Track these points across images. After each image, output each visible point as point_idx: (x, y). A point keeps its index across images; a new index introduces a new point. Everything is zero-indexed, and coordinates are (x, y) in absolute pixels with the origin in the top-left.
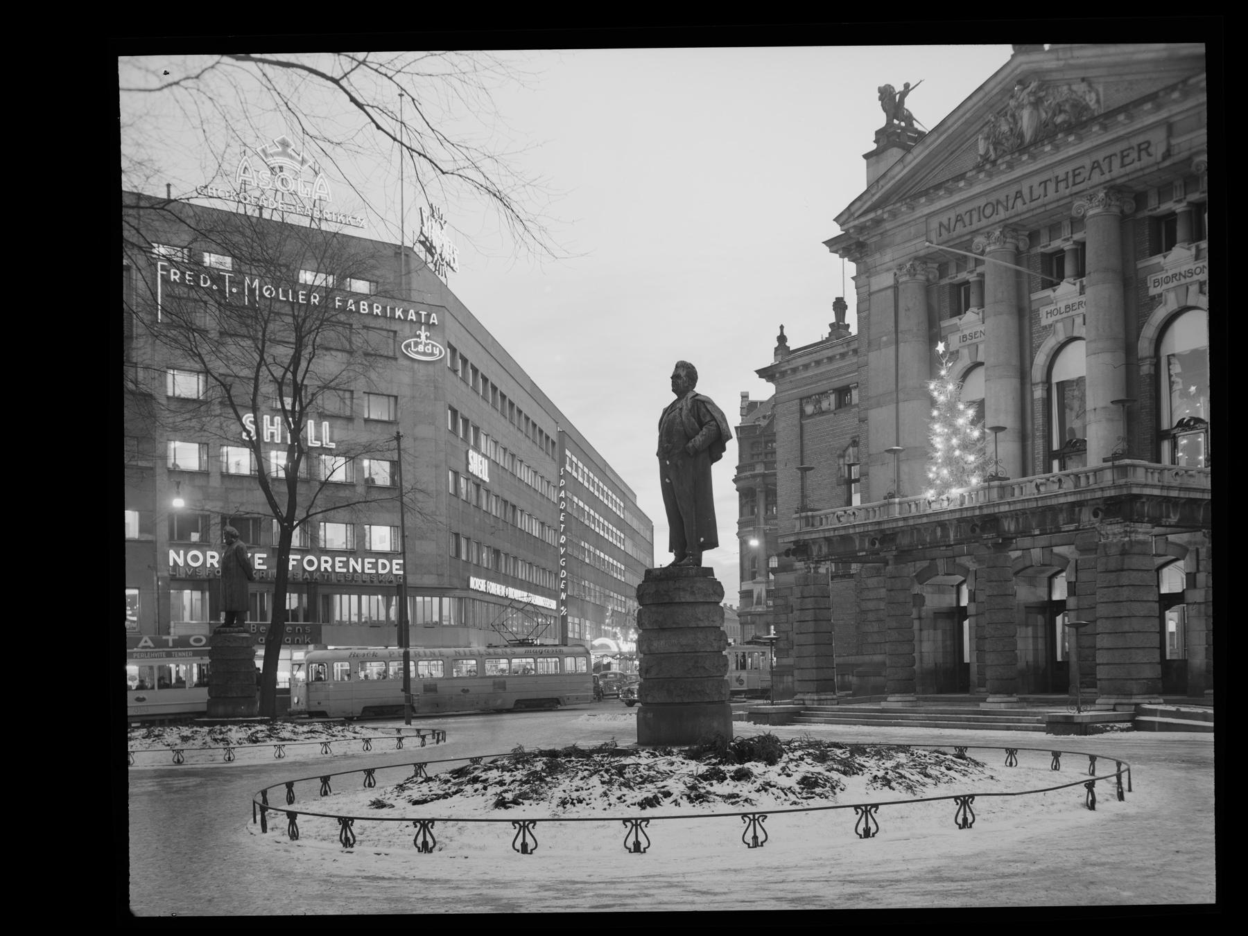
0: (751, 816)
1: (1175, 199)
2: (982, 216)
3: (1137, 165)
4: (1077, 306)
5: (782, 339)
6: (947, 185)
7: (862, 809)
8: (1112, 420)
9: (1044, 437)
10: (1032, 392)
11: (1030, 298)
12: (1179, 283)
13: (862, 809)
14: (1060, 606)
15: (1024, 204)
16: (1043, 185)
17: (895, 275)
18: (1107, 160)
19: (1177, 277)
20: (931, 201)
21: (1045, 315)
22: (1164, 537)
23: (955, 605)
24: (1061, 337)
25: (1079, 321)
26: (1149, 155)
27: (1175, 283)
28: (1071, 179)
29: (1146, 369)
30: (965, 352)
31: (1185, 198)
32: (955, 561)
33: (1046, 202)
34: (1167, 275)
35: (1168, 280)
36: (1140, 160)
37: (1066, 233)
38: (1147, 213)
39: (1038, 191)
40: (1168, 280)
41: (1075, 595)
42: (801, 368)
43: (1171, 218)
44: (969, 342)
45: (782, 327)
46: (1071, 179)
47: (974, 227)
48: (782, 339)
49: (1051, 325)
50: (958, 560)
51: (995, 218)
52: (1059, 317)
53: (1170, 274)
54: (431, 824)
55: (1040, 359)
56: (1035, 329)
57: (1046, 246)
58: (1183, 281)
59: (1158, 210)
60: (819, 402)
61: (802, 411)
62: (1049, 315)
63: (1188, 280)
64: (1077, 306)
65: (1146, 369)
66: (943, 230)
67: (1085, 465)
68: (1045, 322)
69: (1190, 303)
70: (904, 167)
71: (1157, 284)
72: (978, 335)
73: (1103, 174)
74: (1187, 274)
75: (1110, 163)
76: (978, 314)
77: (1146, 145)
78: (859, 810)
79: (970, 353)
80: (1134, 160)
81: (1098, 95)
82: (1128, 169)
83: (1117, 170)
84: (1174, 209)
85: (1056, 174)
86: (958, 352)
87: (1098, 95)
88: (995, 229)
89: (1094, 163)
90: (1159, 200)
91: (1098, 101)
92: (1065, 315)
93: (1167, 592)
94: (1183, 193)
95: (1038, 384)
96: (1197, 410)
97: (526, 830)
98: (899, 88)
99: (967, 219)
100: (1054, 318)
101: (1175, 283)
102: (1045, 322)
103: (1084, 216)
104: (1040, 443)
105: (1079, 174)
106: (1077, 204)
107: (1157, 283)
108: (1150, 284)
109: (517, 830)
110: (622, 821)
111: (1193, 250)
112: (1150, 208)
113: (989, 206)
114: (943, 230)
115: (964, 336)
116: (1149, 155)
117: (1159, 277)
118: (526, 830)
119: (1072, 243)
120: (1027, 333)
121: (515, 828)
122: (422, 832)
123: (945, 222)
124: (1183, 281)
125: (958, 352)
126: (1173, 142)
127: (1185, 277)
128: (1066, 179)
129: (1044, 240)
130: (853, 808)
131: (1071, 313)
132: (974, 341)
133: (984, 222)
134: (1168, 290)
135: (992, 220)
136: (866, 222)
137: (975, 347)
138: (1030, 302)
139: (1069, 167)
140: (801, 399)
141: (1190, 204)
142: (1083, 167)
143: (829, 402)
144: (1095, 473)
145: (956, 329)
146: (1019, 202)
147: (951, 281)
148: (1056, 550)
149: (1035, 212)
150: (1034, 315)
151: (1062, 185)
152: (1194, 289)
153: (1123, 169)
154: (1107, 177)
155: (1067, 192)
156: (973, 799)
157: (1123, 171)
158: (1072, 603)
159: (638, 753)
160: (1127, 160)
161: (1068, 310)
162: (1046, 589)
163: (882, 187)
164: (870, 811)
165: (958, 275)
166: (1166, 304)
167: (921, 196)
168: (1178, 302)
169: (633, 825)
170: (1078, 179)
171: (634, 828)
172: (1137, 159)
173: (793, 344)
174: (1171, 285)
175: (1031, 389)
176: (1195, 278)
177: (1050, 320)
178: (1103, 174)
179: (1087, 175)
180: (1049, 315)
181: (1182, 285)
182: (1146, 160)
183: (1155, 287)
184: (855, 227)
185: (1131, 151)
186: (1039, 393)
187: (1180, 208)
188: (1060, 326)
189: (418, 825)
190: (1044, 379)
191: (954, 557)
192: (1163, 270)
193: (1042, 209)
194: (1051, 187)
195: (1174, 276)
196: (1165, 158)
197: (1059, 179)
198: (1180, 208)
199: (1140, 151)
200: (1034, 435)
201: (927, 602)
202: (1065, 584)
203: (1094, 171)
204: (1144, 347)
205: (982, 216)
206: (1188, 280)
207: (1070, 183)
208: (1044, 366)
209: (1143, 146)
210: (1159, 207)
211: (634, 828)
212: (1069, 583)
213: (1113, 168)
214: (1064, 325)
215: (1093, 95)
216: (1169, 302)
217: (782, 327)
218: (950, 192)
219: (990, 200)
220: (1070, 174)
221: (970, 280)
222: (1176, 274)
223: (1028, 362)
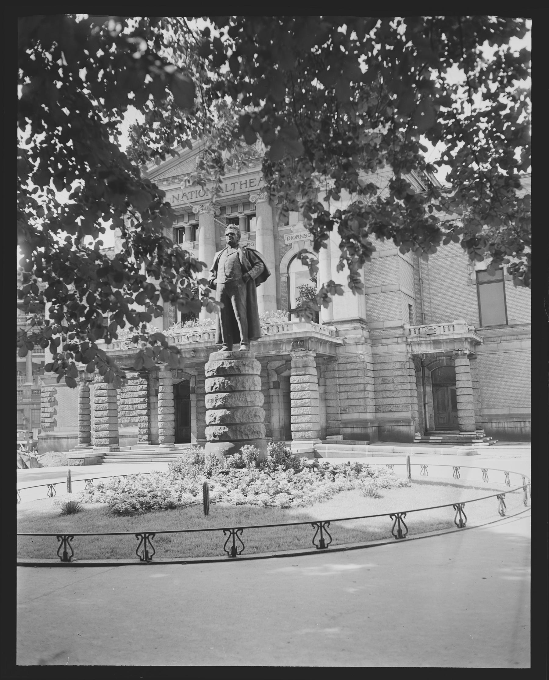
0: (231, 530)
2: (198, 196)
3: (231, 192)
6: (180, 177)
7: (317, 525)
13: (62, 538)
20: (169, 184)
27: (298, 240)
29: (284, 279)
35: (294, 238)
37: (186, 219)
39: (230, 187)
40: (294, 238)
47: (193, 200)
51: (205, 197)
53: (295, 235)
54: (70, 538)
58: (302, 239)
63: (304, 239)
66: (174, 199)
78: (60, 538)
85: (240, 180)
96: (206, 317)
97: (323, 528)
99: (189, 196)
101: (298, 240)
105: (253, 182)
106: (252, 196)
107: (289, 238)
108: (285, 238)
109: (60, 543)
110: (134, 535)
111: (192, 245)
114: (174, 199)
118: (323, 528)
121: (59, 541)
122: (319, 530)
123: (176, 196)
124: (302, 239)
128: (246, 183)
129: (228, 211)
133: (199, 199)
134: (294, 242)
135: (204, 198)
139: (248, 178)
149: (228, 197)
151: (243, 186)
152: (309, 242)
155: (247, 190)
156: (406, 515)
164: (148, 538)
167: (164, 181)
169: (231, 533)
170: (252, 184)
171: (232, 535)
172: (233, 189)
174: (296, 240)
179: (257, 183)
189: (394, 517)
193: (233, 196)
194: (238, 186)
205: (198, 196)
206: (304, 239)
207: (248, 185)
211: (232, 535)
220: (248, 181)
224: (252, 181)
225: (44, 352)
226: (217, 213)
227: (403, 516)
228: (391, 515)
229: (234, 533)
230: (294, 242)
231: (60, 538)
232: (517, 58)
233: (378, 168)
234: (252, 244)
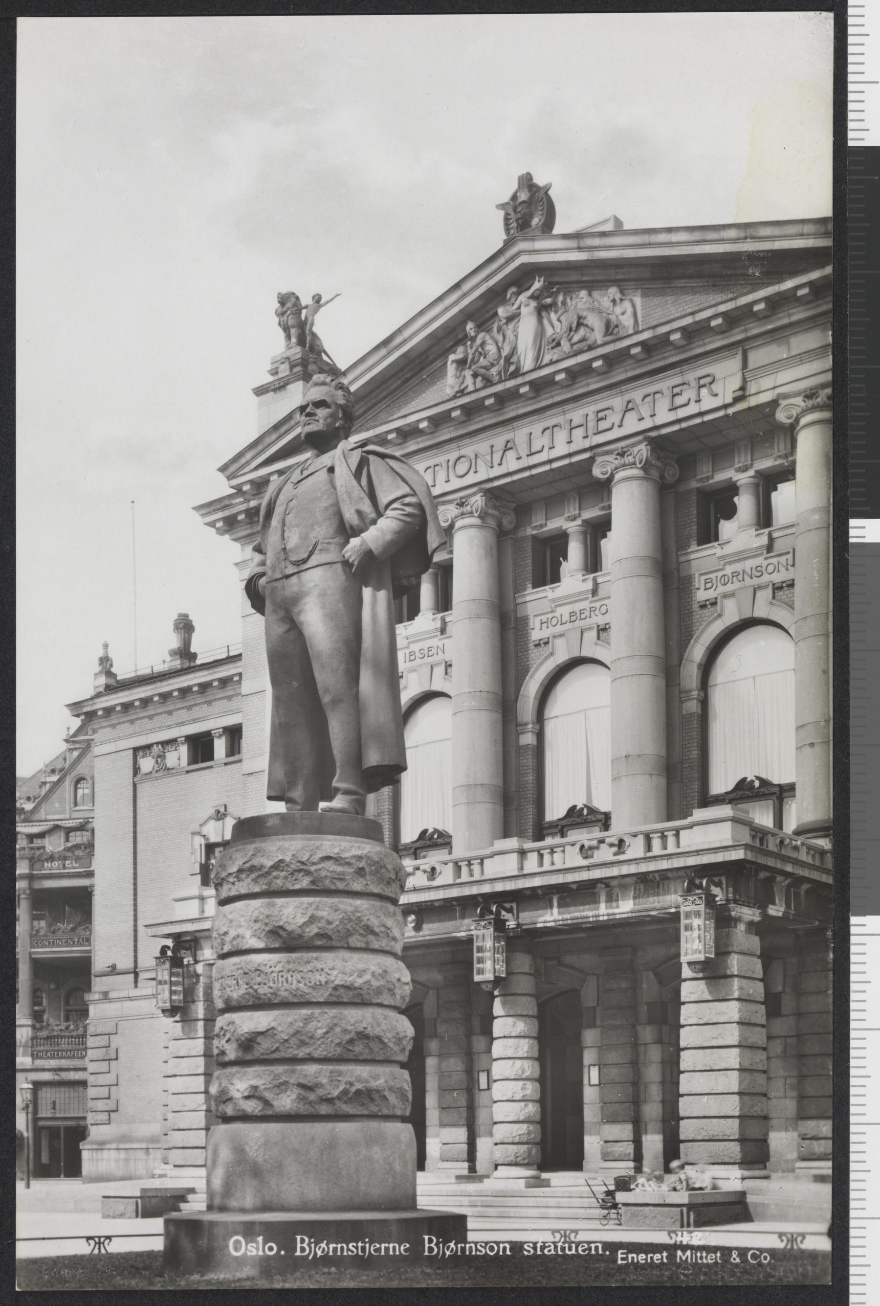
0: (97, 1240)
1: (737, 466)
3: (693, 409)
4: (587, 613)
5: (105, 661)
8: (494, 803)
12: (741, 584)
16: (548, 432)
18: (430, 471)
19: (740, 577)
28: (591, 424)
29: (528, 739)
31: (752, 465)
33: (551, 457)
42: (100, 713)
45: (106, 646)
46: (591, 424)
48: (105, 661)
51: (471, 479)
60: (162, 756)
61: (136, 770)
63: (756, 581)
64: (587, 613)
67: (450, 853)
71: (709, 585)
77: (708, 380)
82: (682, 413)
83: (664, 416)
84: (734, 479)
90: (546, 514)
94: (749, 458)
98: (306, 300)
102: (702, 595)
103: (610, 480)
112: (534, 524)
113: (462, 459)
120: (511, 649)
130: (85, 1240)
131: (578, 623)
133: (455, 483)
134: (725, 596)
136: (419, 421)
140: (136, 750)
143: (179, 756)
144: (482, 860)
146: (511, 455)
153: (673, 412)
154: (647, 424)
155: (587, 444)
157: (672, 417)
160: (679, 401)
161: (573, 618)
168: (740, 611)
169: (96, 1243)
170: (603, 425)
171: (97, 1246)
172: (617, 423)
173: (123, 671)
176: (766, 578)
177: (545, 633)
180: (544, 626)
182: (708, 403)
183: (706, 589)
184: (251, 482)
185: (685, 387)
196: (737, 400)
197: (573, 425)
203: (507, 452)
204: (690, 675)
210: (712, 477)
217: (106, 646)
219: (463, 452)
221: (569, 531)
223: (512, 690)
224: (601, 415)
225: (90, 945)
226: (505, 522)
227: (108, 1241)
228: (89, 1238)
229: (99, 1243)
230: (725, 596)
231: (784, 1238)
232: (833, 377)
233: (473, 704)
234: (603, 609)
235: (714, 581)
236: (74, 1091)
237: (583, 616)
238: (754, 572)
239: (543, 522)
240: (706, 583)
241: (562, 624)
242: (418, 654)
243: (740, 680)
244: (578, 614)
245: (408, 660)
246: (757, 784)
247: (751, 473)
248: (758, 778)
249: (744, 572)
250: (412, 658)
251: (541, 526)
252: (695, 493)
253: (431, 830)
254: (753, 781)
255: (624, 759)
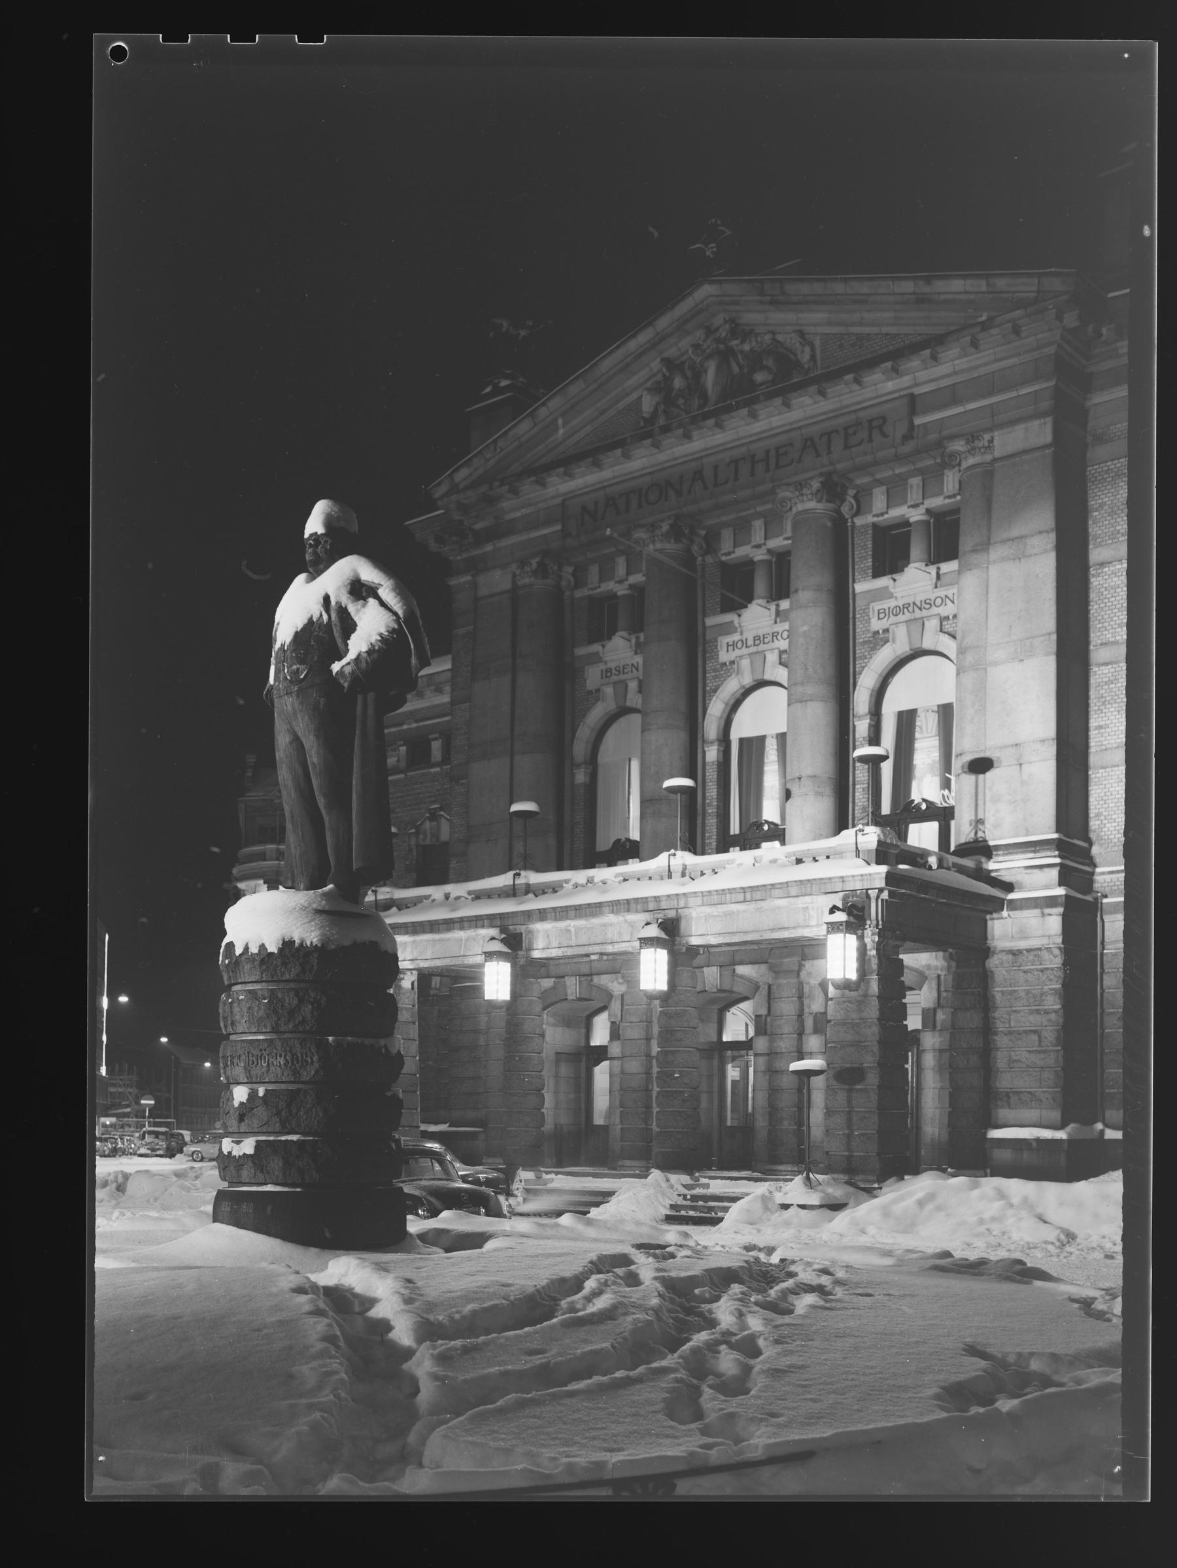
4: (770, 638)
9: (718, 815)
10: (573, 775)
11: (704, 623)
14: (601, 1054)
15: (706, 488)
17: (514, 575)
19: (911, 609)
20: (569, 475)
21: (725, 649)
22: (589, 978)
23: (715, 1039)
24: (747, 680)
25: (772, 658)
26: (884, 435)
30: (609, 691)
32: (592, 980)
34: (896, 603)
36: (870, 440)
38: (870, 519)
41: (765, 1034)
43: (748, 566)
44: (615, 678)
49: (732, 662)
50: (596, 979)
52: (745, 651)
53: (900, 603)
55: (716, 708)
56: (709, 666)
57: (595, 588)
58: (918, 614)
59: (886, 516)
62: (731, 648)
65: (581, 777)
68: (724, 656)
69: (927, 644)
70: (535, 425)
71: (882, 615)
72: (629, 669)
73: (818, 455)
74: (923, 605)
75: (829, 441)
76: (630, 641)
79: (615, 693)
80: (862, 441)
81: (813, 350)
86: (598, 690)
87: (813, 350)
88: (662, 521)
89: (806, 440)
91: (813, 357)
92: (753, 649)
93: (730, 1039)
95: (712, 743)
100: (738, 652)
104: (712, 823)
115: (609, 670)
116: (884, 435)
117: (886, 606)
119: (923, 511)
125: (598, 690)
126: (918, 421)
127: (920, 609)
131: (762, 647)
132: (622, 677)
137: (920, 623)
138: (705, 628)
140: (941, 631)
141: (928, 511)
142: (791, 445)
145: (595, 659)
147: (591, 592)
148: (741, 970)
150: (710, 648)
158: (615, 1050)
159: (740, 1300)
162: (716, 1025)
163: (502, 450)
165: (737, 550)
166: (894, 641)
168: (910, 643)
174: (901, 618)
175: (703, 748)
177: (733, 655)
178: (818, 455)
180: (731, 648)
181: (915, 619)
186: (712, 754)
187: (916, 516)
188: (745, 663)
190: (721, 737)
191: (591, 975)
192: (892, 597)
195: (906, 606)
198: (916, 516)
199: (871, 429)
200: (704, 811)
201: (548, 1038)
202: (608, 1025)
206: (925, 613)
208: (721, 717)
209: (875, 424)
210: (779, 1354)
212: (613, 1023)
213: (832, 449)
214: (752, 663)
215: (807, 349)
216: (898, 641)
218: (598, 465)
220: (773, 453)
222: (909, 604)
224: (781, 451)
235: (887, 612)
236: (1093, 601)
237: (766, 640)
238: (923, 605)
239: (731, 550)
240: (879, 613)
241: (747, 647)
242: (614, 671)
243: (669, 866)
244: (762, 639)
245: (604, 676)
246: (924, 806)
247: (922, 509)
248: (924, 800)
249: (914, 603)
250: (609, 674)
251: (729, 554)
252: (869, 536)
253: (623, 839)
254: (919, 805)
255: (797, 780)
